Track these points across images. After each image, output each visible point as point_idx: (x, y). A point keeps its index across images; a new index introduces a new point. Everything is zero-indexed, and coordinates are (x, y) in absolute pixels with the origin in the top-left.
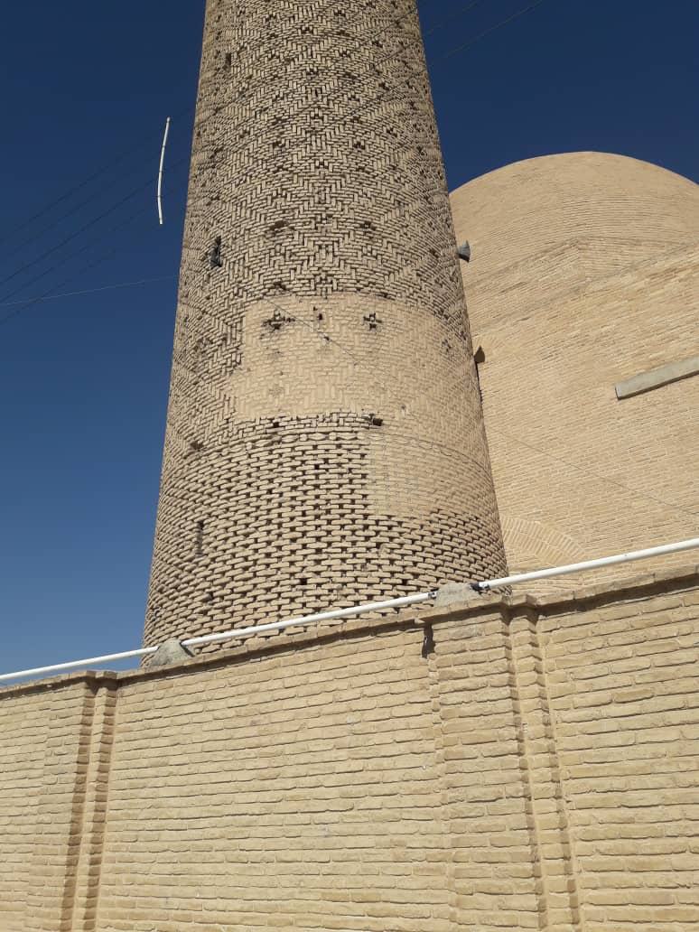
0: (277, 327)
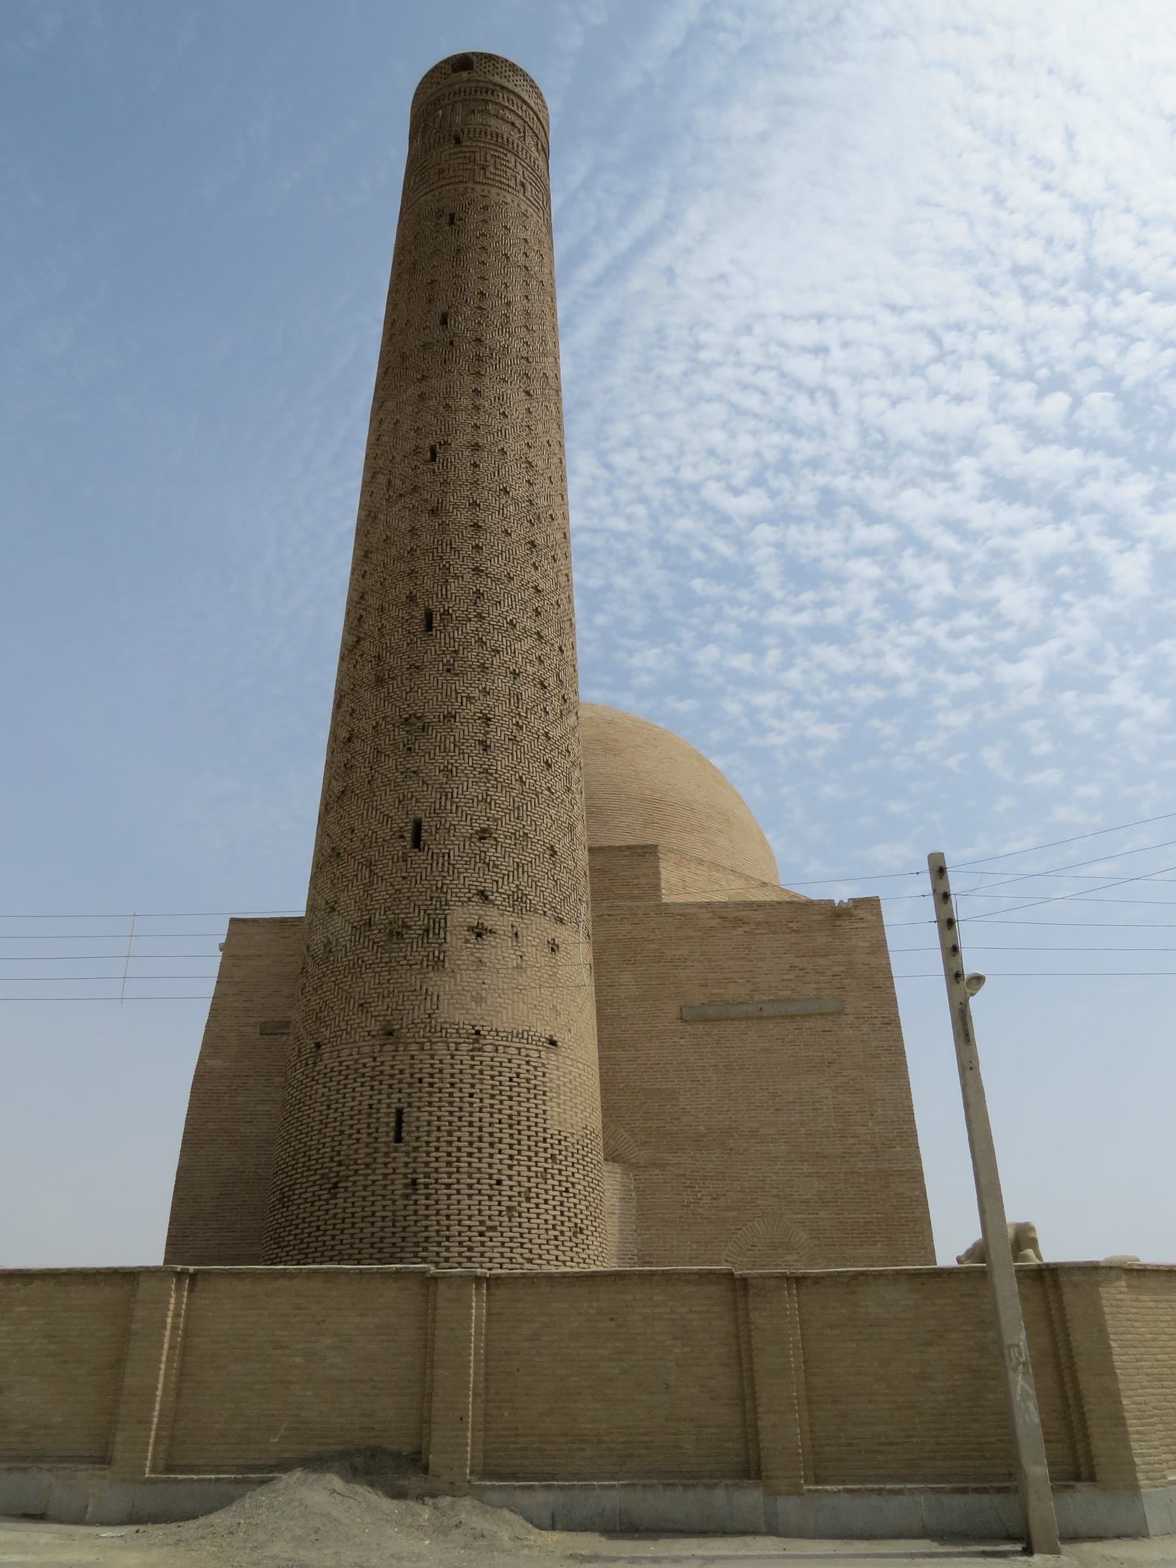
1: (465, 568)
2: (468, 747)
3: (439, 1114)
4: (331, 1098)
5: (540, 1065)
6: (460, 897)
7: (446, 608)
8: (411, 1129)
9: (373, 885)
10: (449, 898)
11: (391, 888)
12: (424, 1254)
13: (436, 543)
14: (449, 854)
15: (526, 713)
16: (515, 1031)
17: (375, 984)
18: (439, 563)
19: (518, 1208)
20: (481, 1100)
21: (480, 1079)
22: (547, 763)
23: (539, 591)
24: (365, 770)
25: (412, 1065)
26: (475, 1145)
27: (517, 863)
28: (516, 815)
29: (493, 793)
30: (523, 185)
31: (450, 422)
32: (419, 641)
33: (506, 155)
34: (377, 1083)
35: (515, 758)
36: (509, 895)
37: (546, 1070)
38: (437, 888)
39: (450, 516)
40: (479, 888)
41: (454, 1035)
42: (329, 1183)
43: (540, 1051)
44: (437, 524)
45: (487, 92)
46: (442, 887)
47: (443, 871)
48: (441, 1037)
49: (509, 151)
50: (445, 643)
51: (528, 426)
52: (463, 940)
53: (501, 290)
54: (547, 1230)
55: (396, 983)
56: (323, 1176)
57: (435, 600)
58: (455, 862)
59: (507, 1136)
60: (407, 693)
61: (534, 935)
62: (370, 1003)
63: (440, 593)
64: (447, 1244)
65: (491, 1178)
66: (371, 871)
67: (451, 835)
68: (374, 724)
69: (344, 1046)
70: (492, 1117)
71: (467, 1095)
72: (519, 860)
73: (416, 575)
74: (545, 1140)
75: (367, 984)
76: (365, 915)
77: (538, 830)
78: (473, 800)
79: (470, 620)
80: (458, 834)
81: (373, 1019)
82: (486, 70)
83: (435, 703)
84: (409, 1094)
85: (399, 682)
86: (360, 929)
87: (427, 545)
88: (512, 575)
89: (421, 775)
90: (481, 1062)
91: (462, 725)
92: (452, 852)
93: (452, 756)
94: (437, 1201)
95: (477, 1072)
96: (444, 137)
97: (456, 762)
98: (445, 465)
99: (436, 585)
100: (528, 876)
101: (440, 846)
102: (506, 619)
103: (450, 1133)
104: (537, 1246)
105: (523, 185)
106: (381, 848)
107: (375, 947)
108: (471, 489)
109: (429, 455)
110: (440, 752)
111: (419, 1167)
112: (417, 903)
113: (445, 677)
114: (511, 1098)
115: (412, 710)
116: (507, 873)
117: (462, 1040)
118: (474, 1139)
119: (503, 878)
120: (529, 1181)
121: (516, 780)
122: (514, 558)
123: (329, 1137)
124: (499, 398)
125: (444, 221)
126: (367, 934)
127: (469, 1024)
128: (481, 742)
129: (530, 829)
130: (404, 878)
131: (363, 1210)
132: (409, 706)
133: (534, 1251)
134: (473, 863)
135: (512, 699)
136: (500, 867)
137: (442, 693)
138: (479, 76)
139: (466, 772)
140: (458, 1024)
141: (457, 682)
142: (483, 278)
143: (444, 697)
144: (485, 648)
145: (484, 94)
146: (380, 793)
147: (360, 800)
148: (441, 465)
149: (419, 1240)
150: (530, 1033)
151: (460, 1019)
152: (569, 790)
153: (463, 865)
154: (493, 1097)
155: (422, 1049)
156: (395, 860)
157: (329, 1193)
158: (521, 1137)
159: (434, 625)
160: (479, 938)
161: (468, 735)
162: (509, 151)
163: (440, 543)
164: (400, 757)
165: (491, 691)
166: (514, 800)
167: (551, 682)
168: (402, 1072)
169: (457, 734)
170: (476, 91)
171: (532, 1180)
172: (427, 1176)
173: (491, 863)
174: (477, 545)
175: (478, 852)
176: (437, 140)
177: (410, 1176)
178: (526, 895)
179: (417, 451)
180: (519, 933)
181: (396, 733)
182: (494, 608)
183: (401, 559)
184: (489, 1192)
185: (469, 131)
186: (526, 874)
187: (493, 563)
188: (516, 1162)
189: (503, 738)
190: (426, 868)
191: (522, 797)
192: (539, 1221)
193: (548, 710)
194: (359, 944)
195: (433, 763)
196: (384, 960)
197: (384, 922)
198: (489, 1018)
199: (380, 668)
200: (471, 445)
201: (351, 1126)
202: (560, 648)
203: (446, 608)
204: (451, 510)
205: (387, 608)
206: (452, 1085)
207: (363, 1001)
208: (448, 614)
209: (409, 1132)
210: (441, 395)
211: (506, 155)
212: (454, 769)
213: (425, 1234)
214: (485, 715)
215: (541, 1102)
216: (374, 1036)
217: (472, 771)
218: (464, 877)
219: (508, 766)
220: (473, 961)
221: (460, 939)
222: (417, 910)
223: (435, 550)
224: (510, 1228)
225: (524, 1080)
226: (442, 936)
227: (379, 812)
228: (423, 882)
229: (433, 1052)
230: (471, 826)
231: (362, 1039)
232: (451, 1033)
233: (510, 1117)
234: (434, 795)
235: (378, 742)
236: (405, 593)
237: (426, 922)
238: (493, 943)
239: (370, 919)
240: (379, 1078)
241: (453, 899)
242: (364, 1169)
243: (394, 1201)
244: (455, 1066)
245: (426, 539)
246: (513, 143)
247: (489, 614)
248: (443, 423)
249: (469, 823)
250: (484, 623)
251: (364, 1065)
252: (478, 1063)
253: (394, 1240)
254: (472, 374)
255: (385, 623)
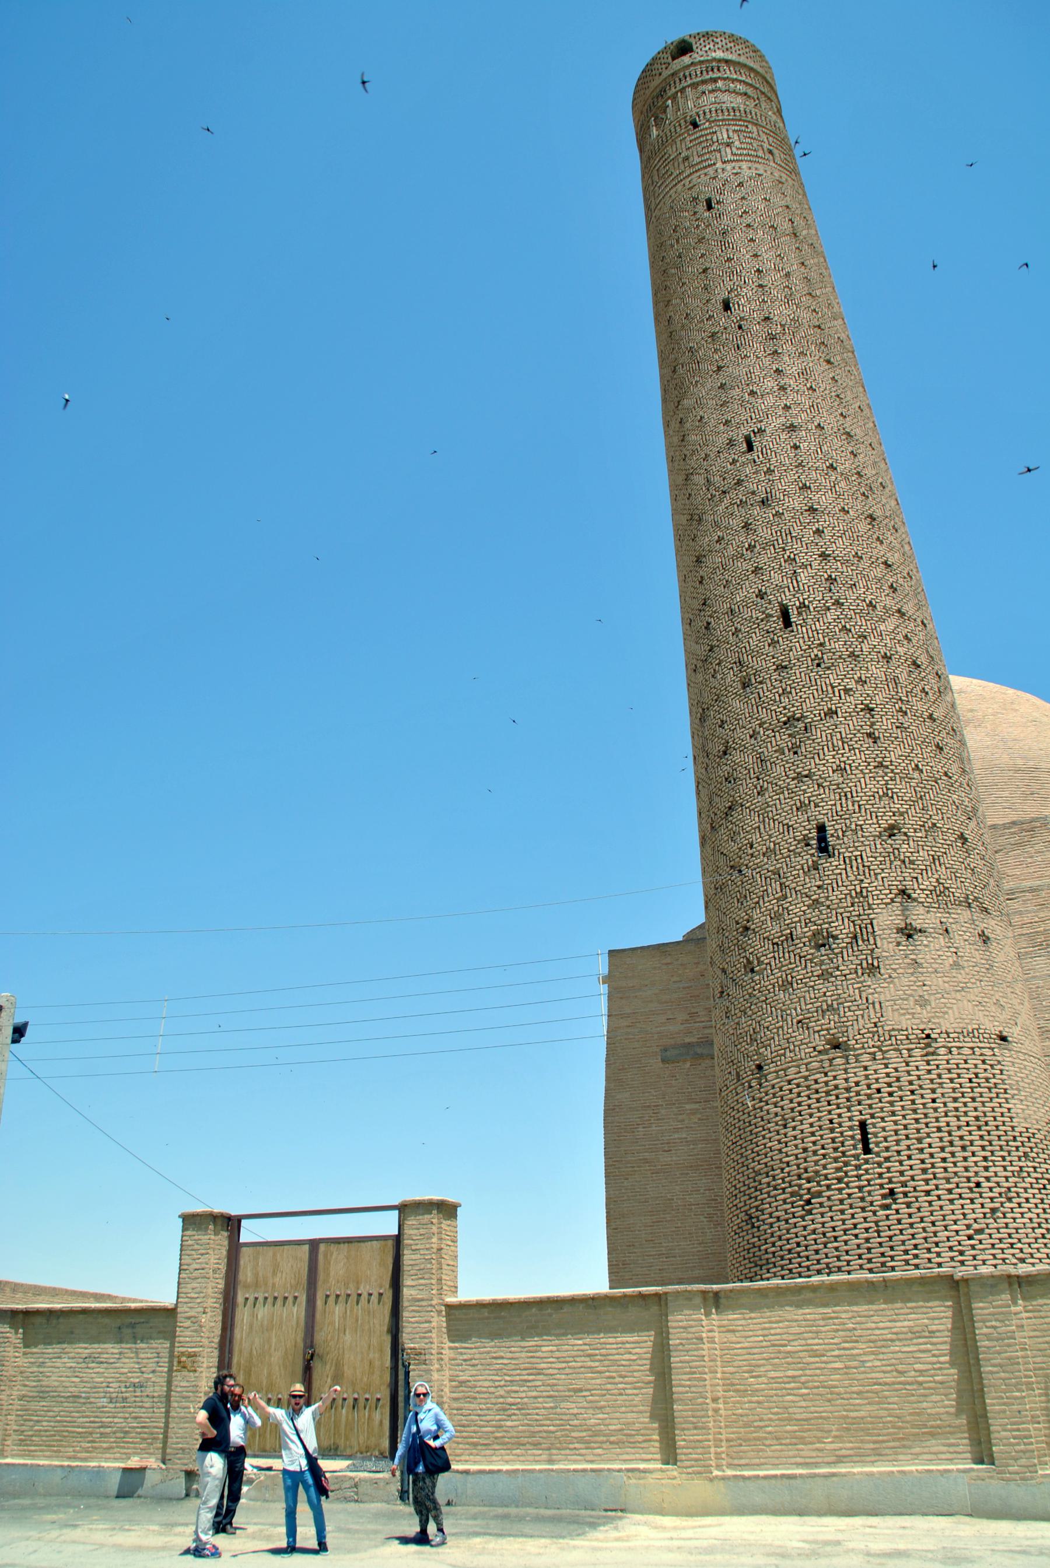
0: (909, 936)
1: (811, 556)
2: (856, 742)
3: (904, 1122)
4: (786, 1116)
5: (996, 1063)
6: (882, 899)
7: (801, 600)
8: (878, 1139)
9: (786, 898)
10: (871, 902)
11: (807, 899)
12: (916, 1261)
13: (774, 535)
14: (861, 855)
15: (907, 696)
16: (965, 1030)
17: (811, 999)
18: (783, 555)
19: (1002, 1209)
20: (945, 1104)
21: (939, 1084)
22: (937, 746)
23: (890, 566)
24: (752, 781)
25: (867, 1077)
26: (947, 1150)
27: (933, 856)
28: (921, 806)
29: (893, 787)
30: (770, 152)
31: (759, 408)
32: (780, 639)
33: (747, 127)
34: (834, 1097)
35: (906, 746)
36: (931, 891)
37: (1002, 1067)
38: (856, 893)
39: (783, 504)
40: (899, 887)
41: (904, 1042)
42: (800, 1200)
43: (992, 1049)
44: (770, 515)
45: (712, 70)
46: (861, 892)
47: (859, 874)
48: (892, 1045)
49: (749, 122)
50: (809, 637)
51: (838, 396)
52: (894, 944)
53: (777, 263)
54: (1033, 1229)
55: (832, 995)
56: (792, 1194)
57: (787, 594)
58: (869, 864)
59: (977, 1138)
60: (780, 696)
61: (963, 929)
62: (809, 1018)
63: (791, 585)
64: (937, 1249)
65: (969, 1181)
66: (781, 884)
67: (860, 836)
68: (751, 733)
69: (790, 1064)
70: (959, 1120)
71: (930, 1101)
72: (933, 853)
73: (760, 571)
74: (1015, 1139)
75: (802, 999)
76: (785, 930)
77: (945, 819)
78: (874, 796)
79: (828, 609)
80: (867, 834)
81: (817, 1034)
82: (707, 48)
83: (812, 702)
84: (870, 1106)
85: (769, 685)
86: (782, 945)
87: (765, 539)
88: (860, 555)
89: (814, 778)
90: (938, 1066)
91: (846, 720)
92: (864, 854)
93: (842, 754)
94: (919, 1209)
95: (935, 1076)
96: (680, 125)
97: (848, 759)
98: (764, 452)
99: (785, 578)
100: (946, 868)
101: (850, 850)
102: (865, 601)
103: (920, 1141)
104: (1027, 1246)
105: (770, 152)
106: (788, 859)
107: (803, 962)
108: (797, 472)
109: (745, 445)
110: (829, 751)
111: (894, 1177)
112: (839, 911)
113: (817, 672)
114: (973, 1099)
115: (789, 712)
116: (924, 867)
117: (913, 1046)
118: (945, 1144)
119: (922, 874)
120: (1007, 1181)
121: (913, 769)
122: (858, 536)
123: (792, 1155)
124: (803, 373)
125: (701, 207)
126: (791, 949)
127: (918, 1029)
128: (869, 735)
129: (937, 818)
130: (819, 887)
131: (844, 1224)
132: (785, 708)
133: (1024, 1251)
134: (888, 862)
135: (890, 684)
136: (917, 863)
137: (817, 690)
138: (702, 56)
139: (860, 768)
140: (907, 1030)
141: (831, 676)
142: (756, 256)
143: (820, 693)
144: (850, 636)
145: (710, 73)
146: (774, 802)
147: (752, 813)
148: (760, 453)
149: (908, 1248)
150: (981, 1031)
151: (907, 1024)
152: (964, 771)
153: (878, 865)
154: (955, 1100)
155: (875, 1059)
156: (806, 870)
157: (803, 1210)
158: (991, 1138)
159: (792, 620)
160: (910, 940)
161: (855, 730)
162: (749, 122)
163: (779, 534)
164: (788, 763)
165: (868, 680)
166: (915, 790)
167: (923, 660)
168: (857, 1084)
169: (843, 730)
170: (701, 73)
171: (1010, 1180)
172: (904, 1184)
173: (907, 859)
174: (818, 530)
175: (891, 850)
176: (673, 130)
177: (886, 1186)
178: (948, 888)
179: (731, 443)
180: (949, 929)
181: (778, 738)
182: (851, 592)
183: (741, 557)
184: (970, 1195)
185: (704, 113)
186: (943, 867)
187: (838, 545)
188: (991, 1164)
189: (890, 727)
190: (841, 874)
191: (922, 786)
192: (1023, 1220)
193: (926, 690)
194: (785, 960)
195: (824, 764)
196: (815, 974)
197: (807, 934)
198: (936, 1021)
199: (745, 673)
200: (787, 428)
201: (814, 1143)
202: (922, 622)
203: (801, 600)
204: (782, 498)
205: (737, 610)
206: (912, 1092)
207: (801, 1017)
208: (805, 606)
209: (877, 1144)
210: (743, 383)
211: (747, 127)
212: (848, 767)
213: (913, 1242)
214: (867, 705)
215: (1004, 1100)
216: (820, 1052)
217: (866, 766)
218: (882, 878)
219: (902, 756)
220: (909, 964)
221: (891, 942)
222: (840, 918)
223: (776, 542)
224: (998, 1229)
225: (983, 1080)
226: (872, 941)
227: (776, 822)
228: (840, 889)
229: (885, 1061)
230: (878, 823)
231: (808, 1055)
232: (901, 1040)
233: (977, 1118)
234: (832, 797)
235: (760, 751)
236: (754, 592)
237: (852, 929)
238: (925, 942)
239: (791, 933)
240: (834, 1092)
241: (875, 902)
242: (836, 1184)
243: (874, 1213)
244: (912, 1073)
245: (764, 533)
246: (751, 113)
247: (846, 599)
248: (752, 410)
249: (875, 821)
250: (844, 609)
251: (816, 1081)
252: (935, 1067)
253: (882, 1250)
254: (769, 354)
255: (739, 626)
